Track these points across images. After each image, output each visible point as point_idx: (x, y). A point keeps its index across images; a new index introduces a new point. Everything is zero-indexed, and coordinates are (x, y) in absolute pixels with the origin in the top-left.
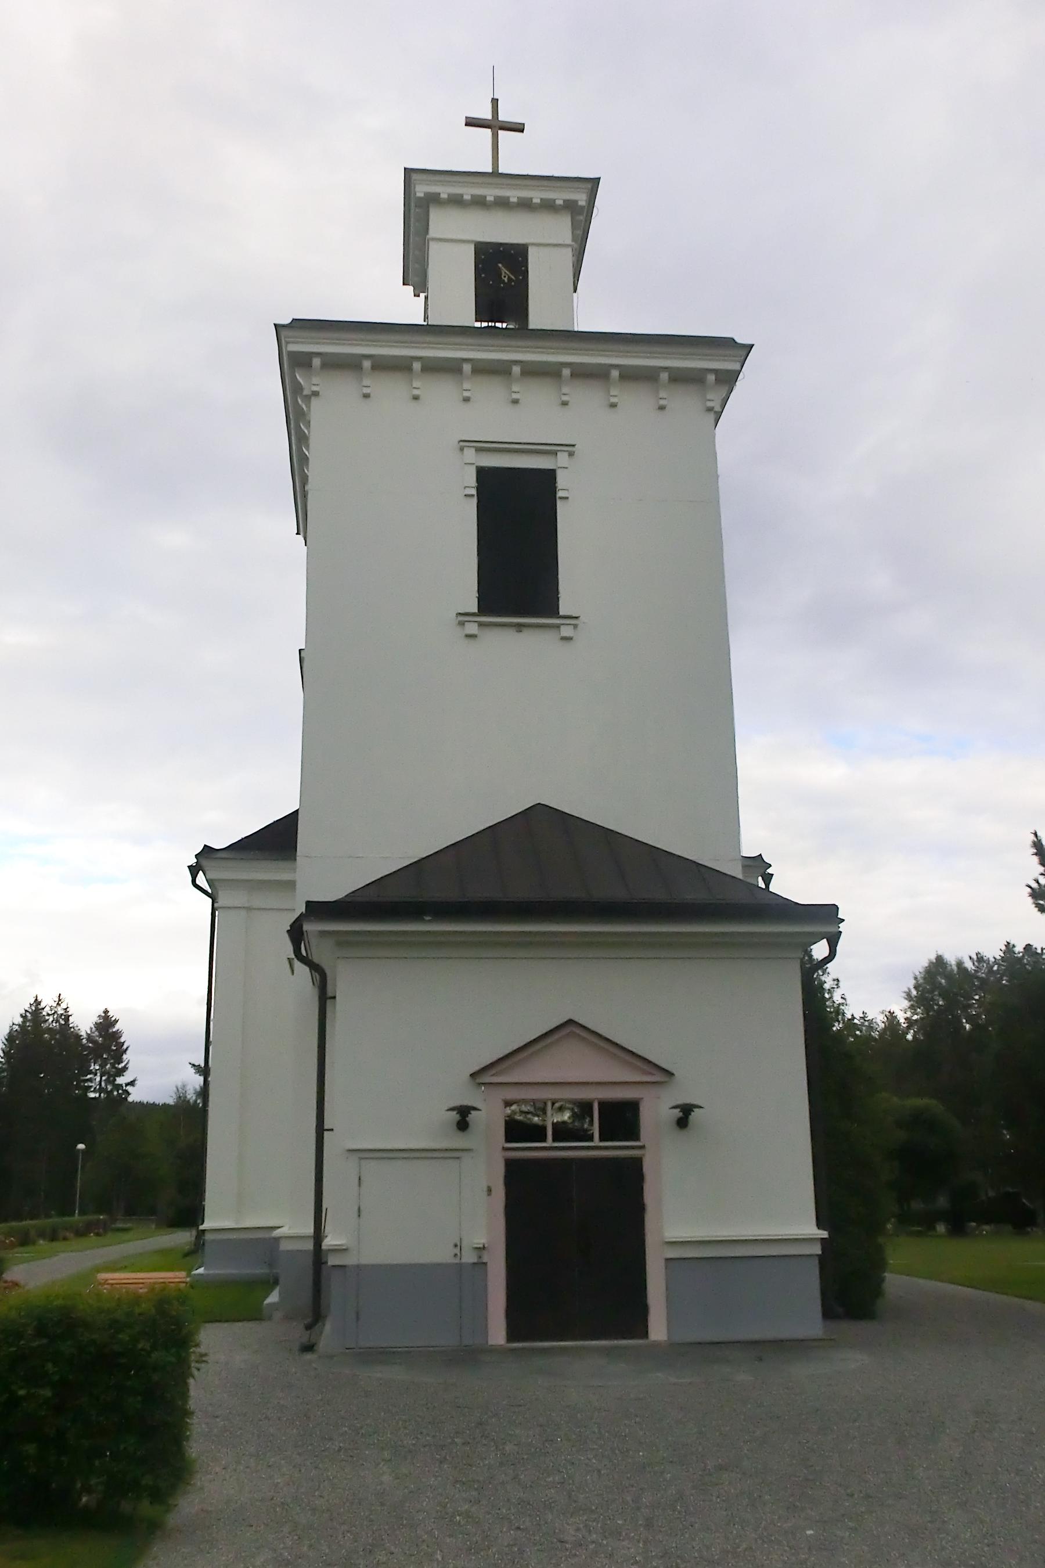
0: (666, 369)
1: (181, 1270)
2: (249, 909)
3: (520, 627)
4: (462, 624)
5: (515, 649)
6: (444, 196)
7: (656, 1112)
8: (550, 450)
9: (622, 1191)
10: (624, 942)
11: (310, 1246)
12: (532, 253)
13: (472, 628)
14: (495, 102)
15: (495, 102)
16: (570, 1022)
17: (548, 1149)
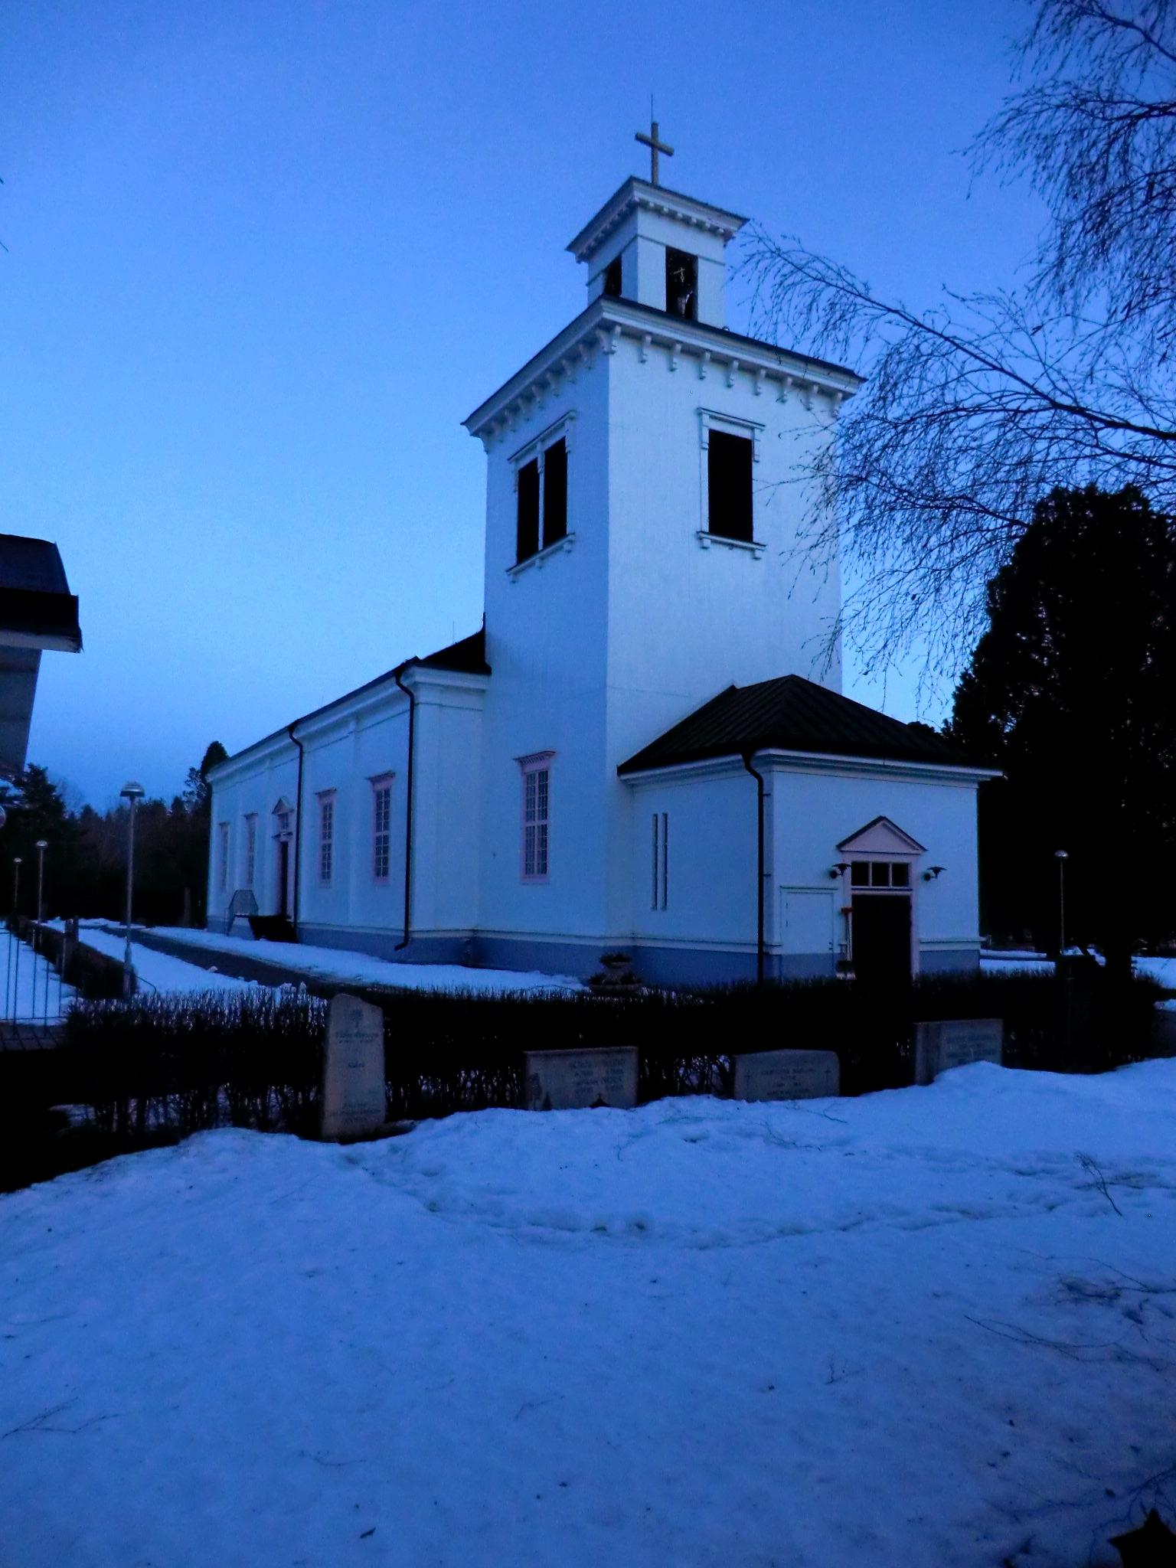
0: (680, 342)
1: (90, 951)
2: (441, 706)
3: (732, 546)
4: (701, 539)
5: (724, 557)
6: (680, 215)
7: (918, 868)
8: (751, 426)
9: (900, 912)
10: (821, 765)
11: (756, 950)
12: (700, 262)
13: (707, 542)
14: (654, 126)
15: (654, 126)
16: (881, 818)
17: (871, 890)
